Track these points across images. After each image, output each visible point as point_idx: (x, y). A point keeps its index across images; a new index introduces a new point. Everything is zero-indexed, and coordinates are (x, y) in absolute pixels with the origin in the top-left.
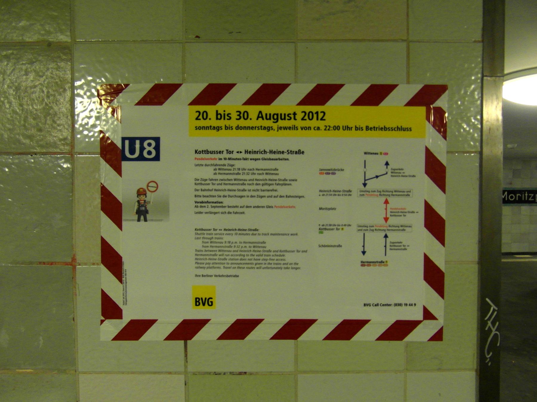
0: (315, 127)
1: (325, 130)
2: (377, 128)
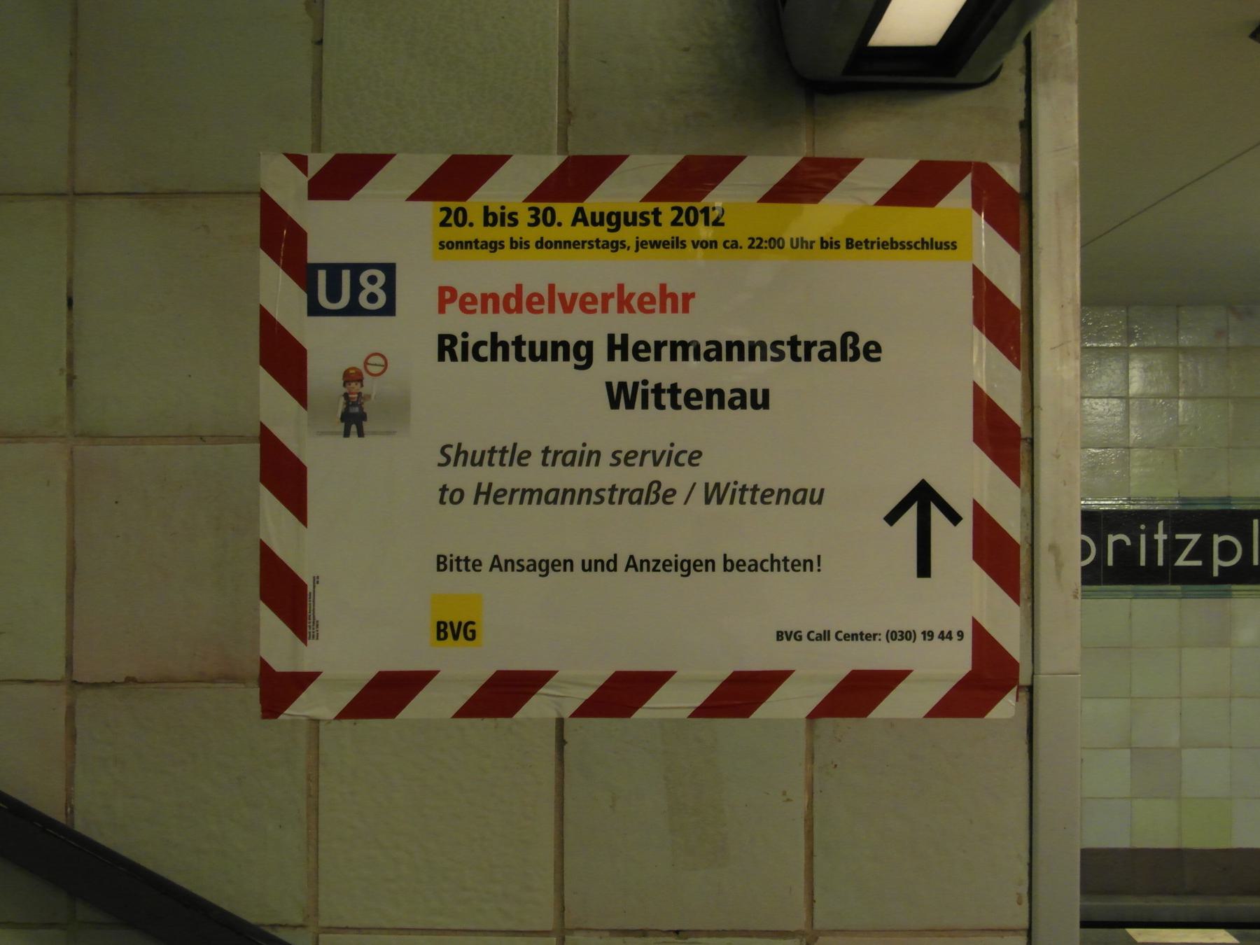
0: (728, 241)
1: (750, 247)
2: (873, 243)
